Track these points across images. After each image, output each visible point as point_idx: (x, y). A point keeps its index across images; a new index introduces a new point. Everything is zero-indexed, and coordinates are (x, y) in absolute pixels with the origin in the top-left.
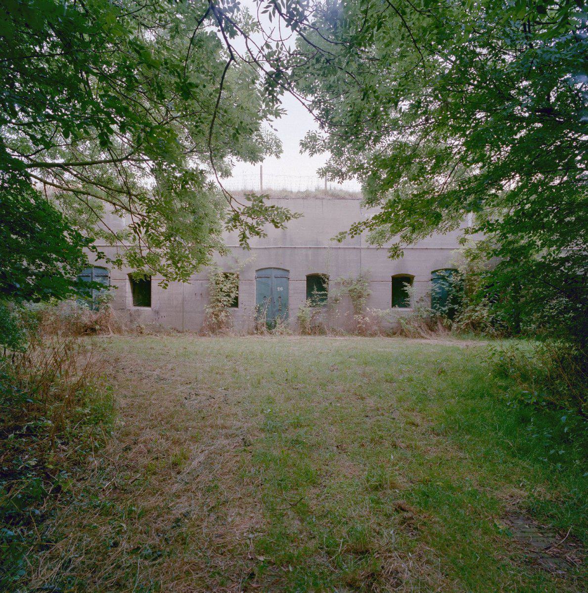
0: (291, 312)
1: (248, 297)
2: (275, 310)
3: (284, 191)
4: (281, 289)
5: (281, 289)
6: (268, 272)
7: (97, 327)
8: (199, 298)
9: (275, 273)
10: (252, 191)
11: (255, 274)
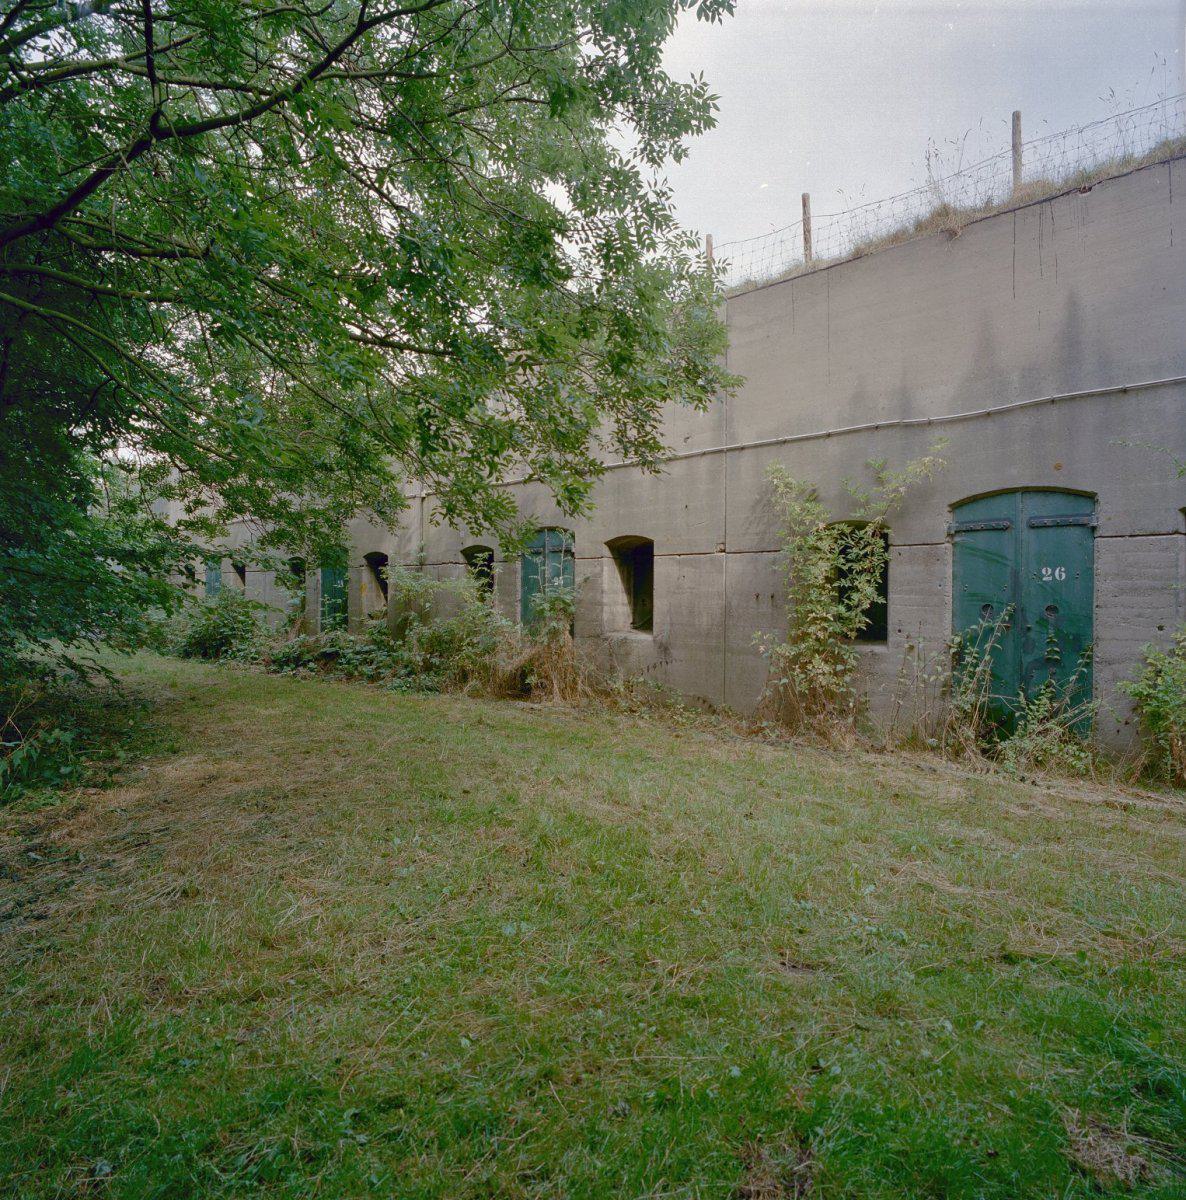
0: (1101, 675)
1: (926, 607)
2: (1028, 659)
3: (748, 282)
4: (1060, 574)
5: (1060, 574)
6: (1000, 509)
7: (532, 680)
8: (765, 607)
9: (1033, 508)
10: (743, 280)
11: (945, 521)
